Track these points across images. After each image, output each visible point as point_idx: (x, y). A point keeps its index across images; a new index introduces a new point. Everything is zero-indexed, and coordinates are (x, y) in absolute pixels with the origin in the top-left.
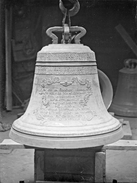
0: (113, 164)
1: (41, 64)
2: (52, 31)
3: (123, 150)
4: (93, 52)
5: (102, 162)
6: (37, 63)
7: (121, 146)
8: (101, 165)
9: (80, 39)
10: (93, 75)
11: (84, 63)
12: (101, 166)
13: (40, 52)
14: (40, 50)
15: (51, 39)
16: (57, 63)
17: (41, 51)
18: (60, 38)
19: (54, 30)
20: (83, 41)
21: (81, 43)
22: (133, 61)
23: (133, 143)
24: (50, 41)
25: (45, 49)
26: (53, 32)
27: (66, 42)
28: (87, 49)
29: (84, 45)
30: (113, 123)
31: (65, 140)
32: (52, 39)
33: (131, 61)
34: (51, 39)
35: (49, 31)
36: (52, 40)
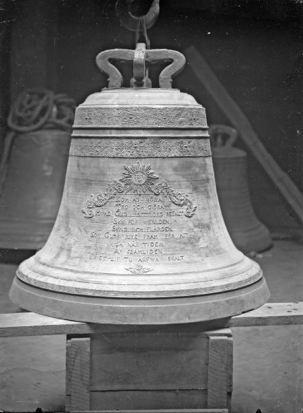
0: (260, 365)
1: (152, 134)
2: (109, 57)
3: (265, 325)
4: (201, 107)
5: (226, 359)
6: (74, 132)
7: (260, 318)
8: (224, 366)
9: (172, 79)
10: (154, 159)
11: (95, 131)
12: (223, 369)
13: (80, 106)
14: (82, 101)
15: (107, 76)
16: (195, 132)
17: (83, 104)
18: (131, 77)
19: (117, 57)
20: (179, 83)
21: (174, 86)
22: (220, 131)
23: (297, 309)
24: (102, 83)
25: (94, 100)
26: (111, 60)
27: (140, 83)
28: (189, 100)
29: (181, 91)
30: (248, 268)
31: (106, 304)
32: (108, 77)
33: (217, 129)
34: (107, 76)
35: (102, 59)
36: (109, 79)
